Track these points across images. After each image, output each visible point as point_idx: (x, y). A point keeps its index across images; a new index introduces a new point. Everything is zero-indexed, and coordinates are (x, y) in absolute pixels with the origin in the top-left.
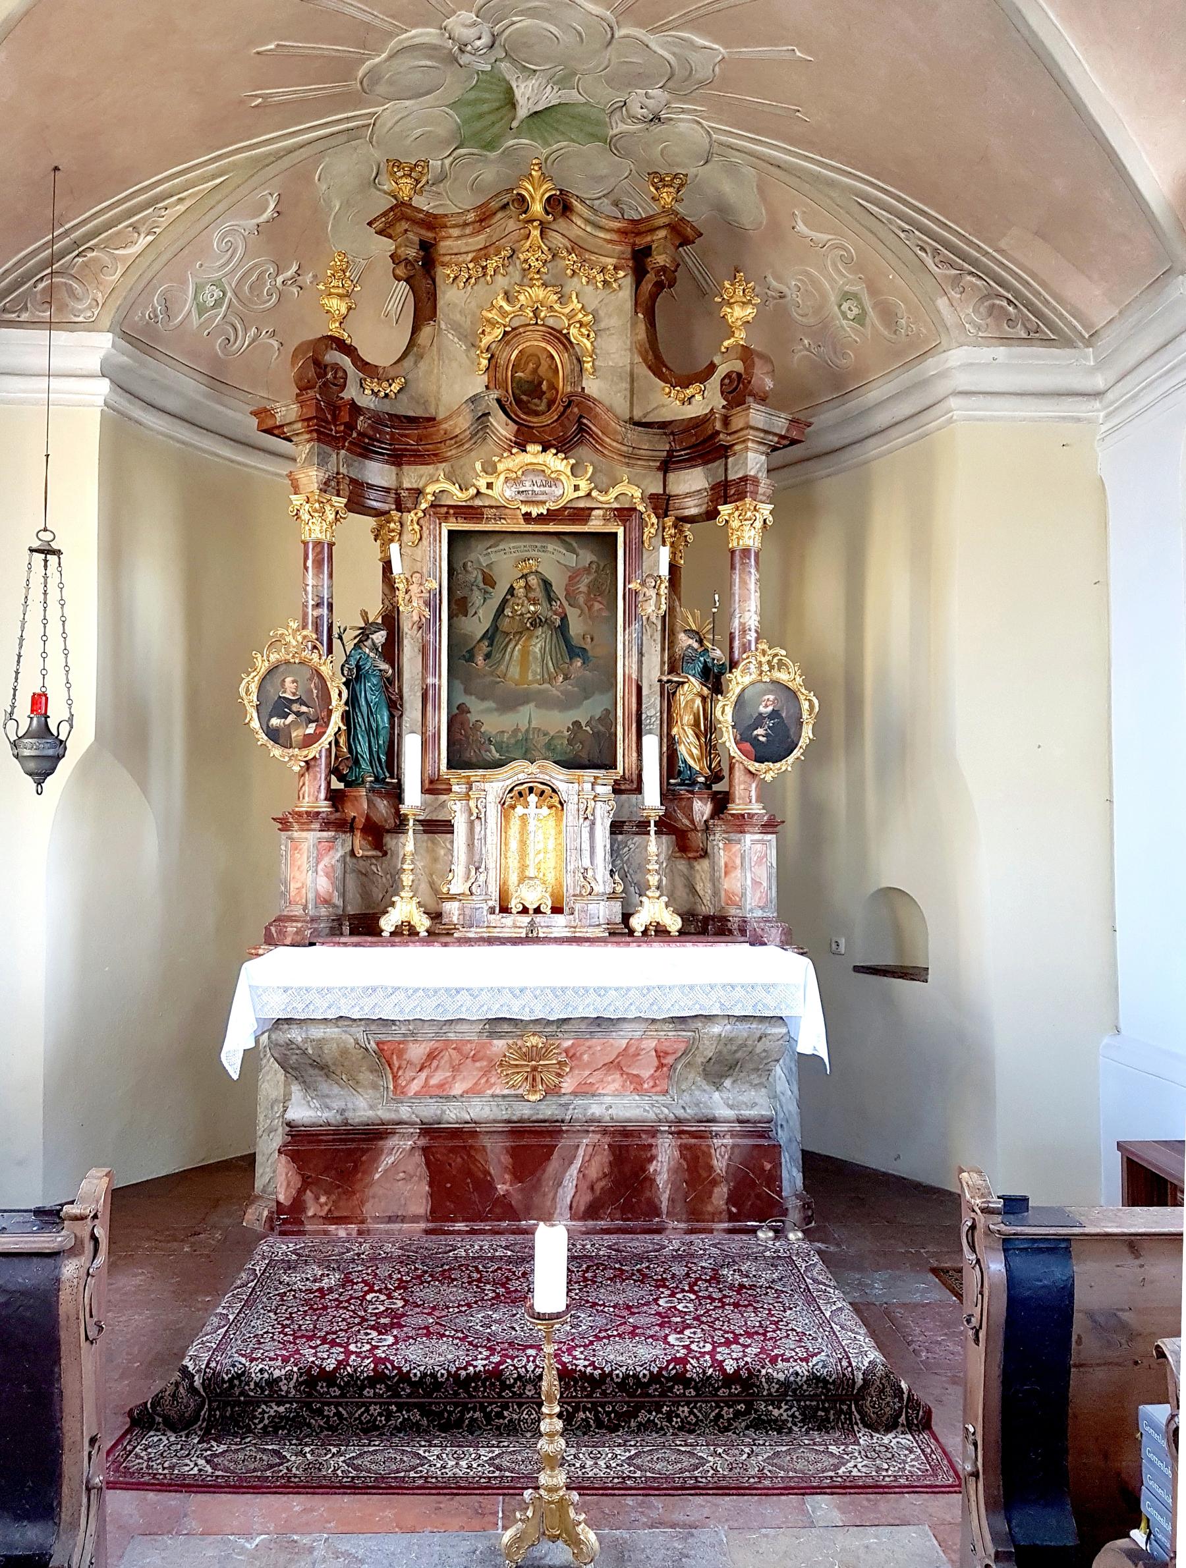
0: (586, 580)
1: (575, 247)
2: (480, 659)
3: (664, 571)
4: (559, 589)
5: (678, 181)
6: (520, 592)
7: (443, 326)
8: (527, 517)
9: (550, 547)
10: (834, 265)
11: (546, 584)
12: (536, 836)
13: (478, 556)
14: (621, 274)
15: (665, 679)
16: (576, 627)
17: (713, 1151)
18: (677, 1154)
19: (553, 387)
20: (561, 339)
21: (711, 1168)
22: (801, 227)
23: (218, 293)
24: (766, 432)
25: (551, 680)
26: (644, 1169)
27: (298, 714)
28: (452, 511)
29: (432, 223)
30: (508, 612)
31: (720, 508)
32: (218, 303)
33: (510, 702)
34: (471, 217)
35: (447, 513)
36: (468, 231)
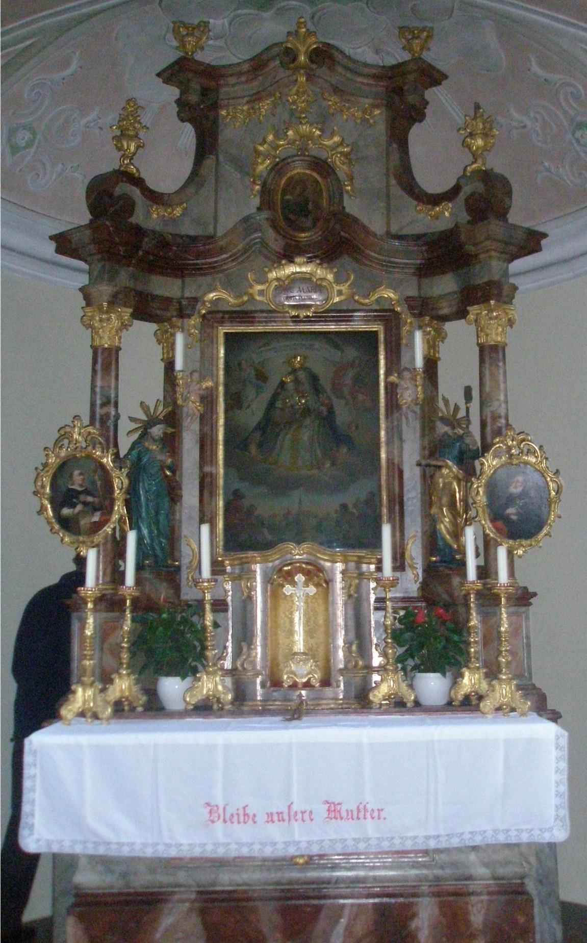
0: (351, 373)
1: (337, 90)
2: (253, 449)
3: (419, 363)
4: (325, 382)
5: (425, 34)
6: (290, 386)
7: (221, 158)
8: (296, 320)
9: (317, 345)
10: (566, 100)
11: (314, 379)
12: (301, 611)
13: (253, 355)
14: (377, 112)
15: (424, 463)
16: (343, 415)
17: (470, 907)
18: (436, 911)
19: (317, 206)
20: (322, 166)
21: (468, 923)
22: (536, 68)
23: (28, 135)
24: (506, 243)
25: (319, 466)
26: (405, 926)
27: (85, 504)
28: (227, 316)
29: (212, 74)
30: (279, 404)
31: (468, 308)
32: (29, 145)
33: (283, 486)
34: (246, 67)
35: (223, 318)
36: (243, 79)
